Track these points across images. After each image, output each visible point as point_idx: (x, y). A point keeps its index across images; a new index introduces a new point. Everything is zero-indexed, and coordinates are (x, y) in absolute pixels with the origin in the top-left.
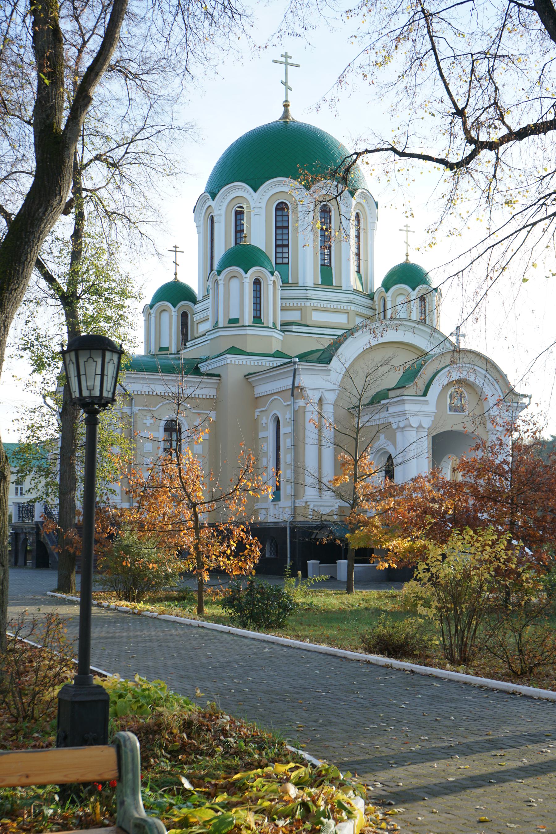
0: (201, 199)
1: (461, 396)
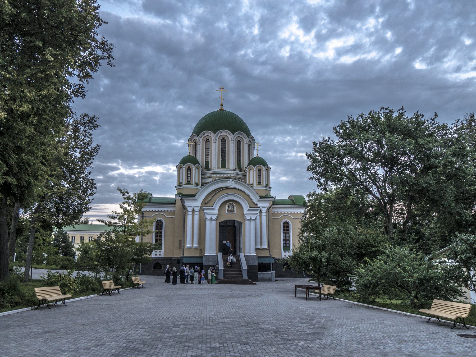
0: (192, 137)
1: (233, 206)
